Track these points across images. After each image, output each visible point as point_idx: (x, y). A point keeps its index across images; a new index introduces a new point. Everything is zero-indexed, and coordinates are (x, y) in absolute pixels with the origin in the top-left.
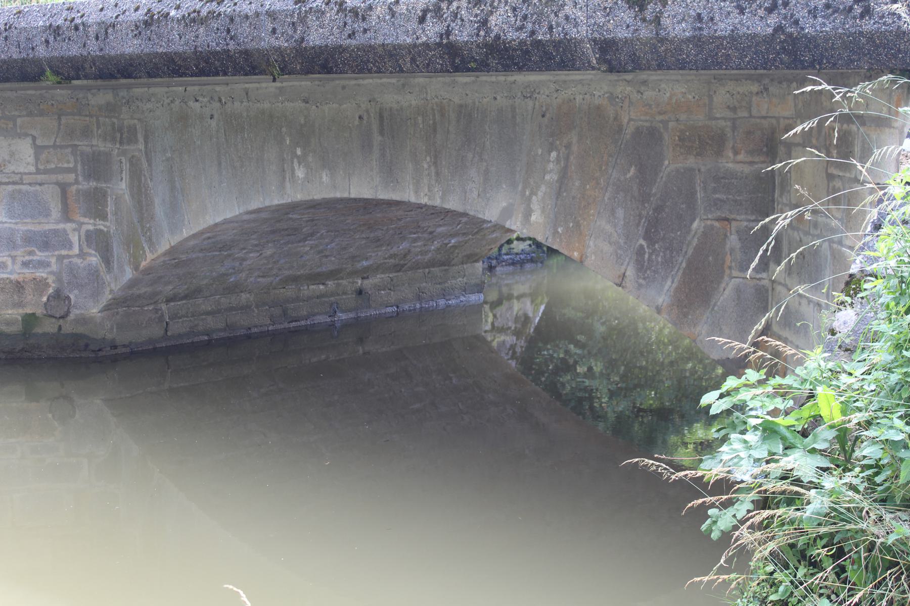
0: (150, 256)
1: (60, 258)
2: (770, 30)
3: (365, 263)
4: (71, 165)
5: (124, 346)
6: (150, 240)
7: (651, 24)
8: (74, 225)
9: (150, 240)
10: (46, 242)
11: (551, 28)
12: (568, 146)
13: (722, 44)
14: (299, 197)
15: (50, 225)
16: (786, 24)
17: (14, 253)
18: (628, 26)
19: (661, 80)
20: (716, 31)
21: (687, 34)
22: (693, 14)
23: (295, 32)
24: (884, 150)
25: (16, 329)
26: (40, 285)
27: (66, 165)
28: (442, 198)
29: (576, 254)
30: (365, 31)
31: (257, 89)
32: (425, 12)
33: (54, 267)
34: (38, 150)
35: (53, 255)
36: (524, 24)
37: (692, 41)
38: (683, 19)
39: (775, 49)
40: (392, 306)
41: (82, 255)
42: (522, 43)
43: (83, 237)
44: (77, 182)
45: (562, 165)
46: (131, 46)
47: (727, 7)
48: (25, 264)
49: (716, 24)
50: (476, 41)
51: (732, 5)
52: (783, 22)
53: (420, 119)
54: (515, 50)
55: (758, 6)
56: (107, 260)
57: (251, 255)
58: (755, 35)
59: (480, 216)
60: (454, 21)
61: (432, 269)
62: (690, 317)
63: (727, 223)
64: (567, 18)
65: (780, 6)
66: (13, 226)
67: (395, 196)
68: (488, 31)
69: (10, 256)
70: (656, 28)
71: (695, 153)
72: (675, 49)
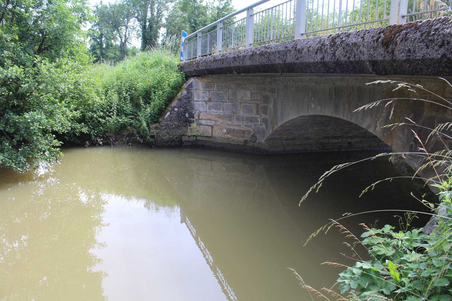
0: (276, 127)
1: (255, 125)
2: (439, 56)
3: (351, 135)
4: (260, 99)
5: (271, 152)
6: (276, 122)
7: (390, 54)
8: (259, 116)
10: (252, 120)
11: (355, 56)
13: (419, 63)
15: (254, 115)
16: (447, 53)
17: (243, 122)
18: (382, 55)
19: (426, 81)
20: (416, 57)
21: (404, 58)
22: (407, 49)
23: (284, 58)
24: (446, 125)
25: (242, 144)
26: (249, 132)
27: (258, 99)
28: (351, 118)
29: (389, 144)
30: (301, 57)
31: (304, 78)
32: (317, 50)
33: (253, 128)
34: (252, 94)
35: (253, 124)
36: (346, 54)
37: (406, 61)
38: (403, 52)
39: (442, 65)
40: (360, 148)
41: (261, 125)
42: (346, 62)
43: (262, 120)
44: (261, 104)
45: (388, 111)
46: (248, 63)
47: (422, 46)
48: (246, 126)
49: (416, 54)
50: (331, 61)
51: (424, 44)
52: (446, 52)
53: (346, 90)
54: (344, 65)
55: (435, 44)
56: (267, 127)
57: (310, 129)
58: (433, 59)
59: (361, 126)
60: (325, 53)
61: (375, 138)
62: (427, 174)
63: (445, 140)
64: (360, 51)
65: (445, 44)
66: (243, 115)
67: (337, 117)
68: (335, 57)
69: (242, 123)
70: (392, 56)
71: (436, 110)
72: (400, 65)
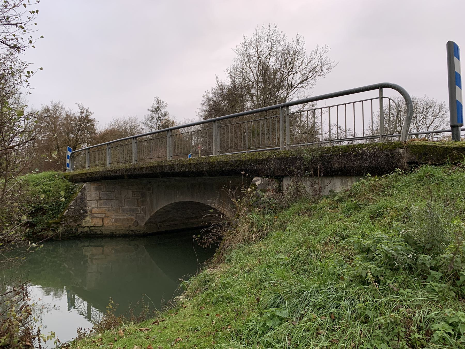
1: (136, 214)
9: (153, 210)
14: (177, 201)
34: (133, 192)
41: (141, 213)
44: (140, 199)
67: (193, 201)
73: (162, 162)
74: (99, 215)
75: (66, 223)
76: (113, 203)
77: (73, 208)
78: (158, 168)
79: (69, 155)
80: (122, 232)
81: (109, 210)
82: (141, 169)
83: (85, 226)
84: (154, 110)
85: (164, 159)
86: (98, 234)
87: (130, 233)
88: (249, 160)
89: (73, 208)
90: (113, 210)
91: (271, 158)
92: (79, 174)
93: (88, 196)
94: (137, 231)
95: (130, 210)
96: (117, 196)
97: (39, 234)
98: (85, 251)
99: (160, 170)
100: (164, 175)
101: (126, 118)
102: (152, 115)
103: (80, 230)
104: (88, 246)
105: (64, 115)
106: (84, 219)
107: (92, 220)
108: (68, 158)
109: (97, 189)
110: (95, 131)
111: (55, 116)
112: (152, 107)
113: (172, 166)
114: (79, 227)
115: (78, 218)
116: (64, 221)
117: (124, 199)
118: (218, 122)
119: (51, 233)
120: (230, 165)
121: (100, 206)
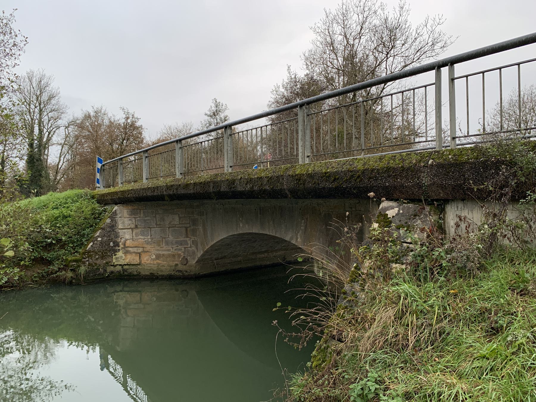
1: (185, 248)
12: (307, 219)
14: (241, 232)
34: (180, 218)
41: (191, 247)
44: (190, 226)
46: (182, 191)
67: (264, 233)
73: (216, 175)
74: (135, 250)
75: (90, 260)
76: (153, 232)
77: (99, 239)
78: (212, 185)
79: (100, 168)
80: (165, 273)
81: (148, 243)
82: (187, 186)
83: (115, 264)
84: (212, 114)
85: (220, 171)
86: (134, 275)
87: (177, 274)
88: (373, 170)
89: (99, 239)
90: (154, 243)
91: (422, 164)
92: (109, 194)
93: (120, 223)
94: (186, 271)
95: (176, 243)
96: (158, 223)
97: (55, 275)
98: (117, 299)
99: (213, 187)
100: (221, 195)
101: (180, 126)
102: (209, 120)
103: (110, 269)
104: (121, 291)
105: (106, 122)
106: (115, 255)
107: (125, 256)
108: (98, 172)
109: (133, 213)
110: (142, 141)
111: (96, 123)
112: (210, 111)
113: (232, 182)
114: (109, 266)
115: (106, 253)
116: (88, 257)
117: (169, 228)
118: (307, 107)
119: (70, 274)
120: (333, 179)
121: (136, 236)
